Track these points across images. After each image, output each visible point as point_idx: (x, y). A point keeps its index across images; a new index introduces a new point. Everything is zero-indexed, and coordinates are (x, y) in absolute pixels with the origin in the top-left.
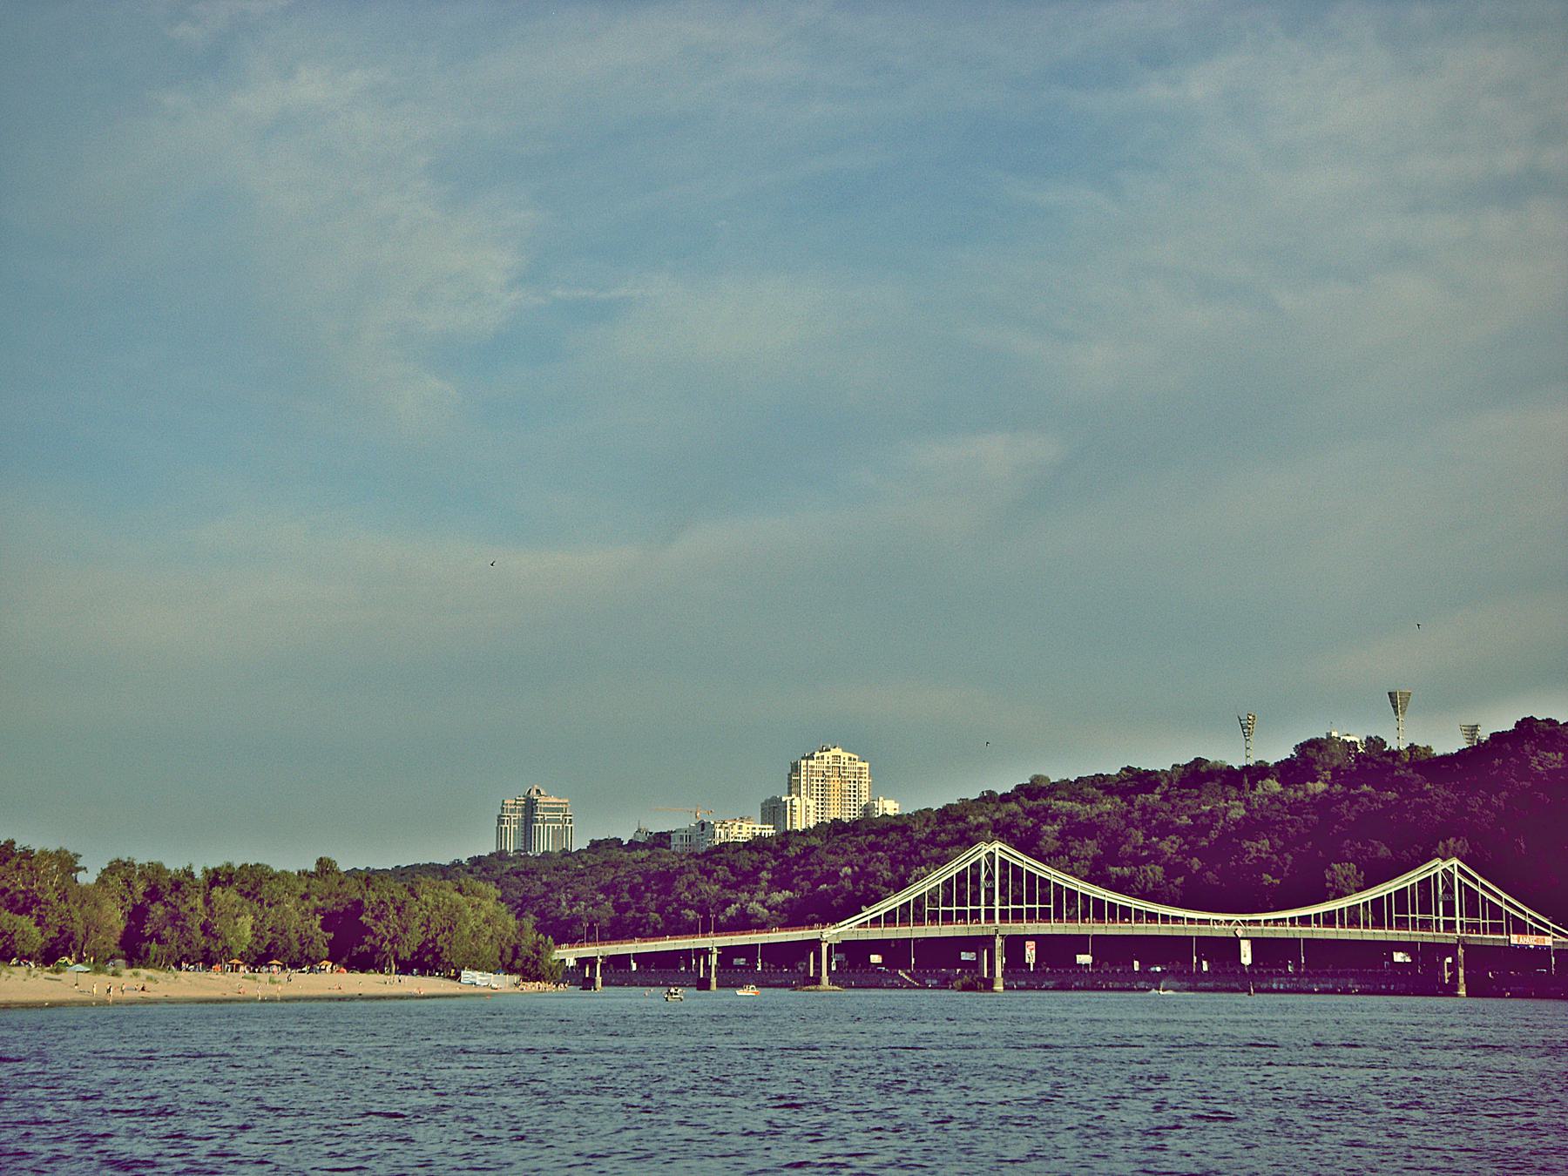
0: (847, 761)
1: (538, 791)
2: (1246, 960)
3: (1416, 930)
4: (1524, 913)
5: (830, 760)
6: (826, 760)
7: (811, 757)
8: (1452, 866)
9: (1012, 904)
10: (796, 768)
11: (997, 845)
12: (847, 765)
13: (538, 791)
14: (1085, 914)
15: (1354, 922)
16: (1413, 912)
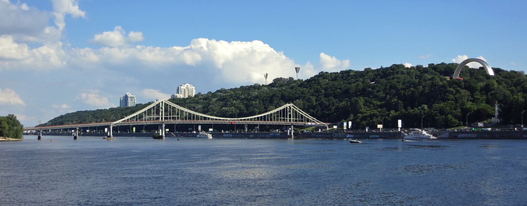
1: (128, 94)
2: (400, 122)
4: (309, 117)
5: (186, 86)
6: (185, 86)
7: (182, 86)
8: (291, 105)
9: (169, 116)
13: (128, 94)
14: (194, 119)
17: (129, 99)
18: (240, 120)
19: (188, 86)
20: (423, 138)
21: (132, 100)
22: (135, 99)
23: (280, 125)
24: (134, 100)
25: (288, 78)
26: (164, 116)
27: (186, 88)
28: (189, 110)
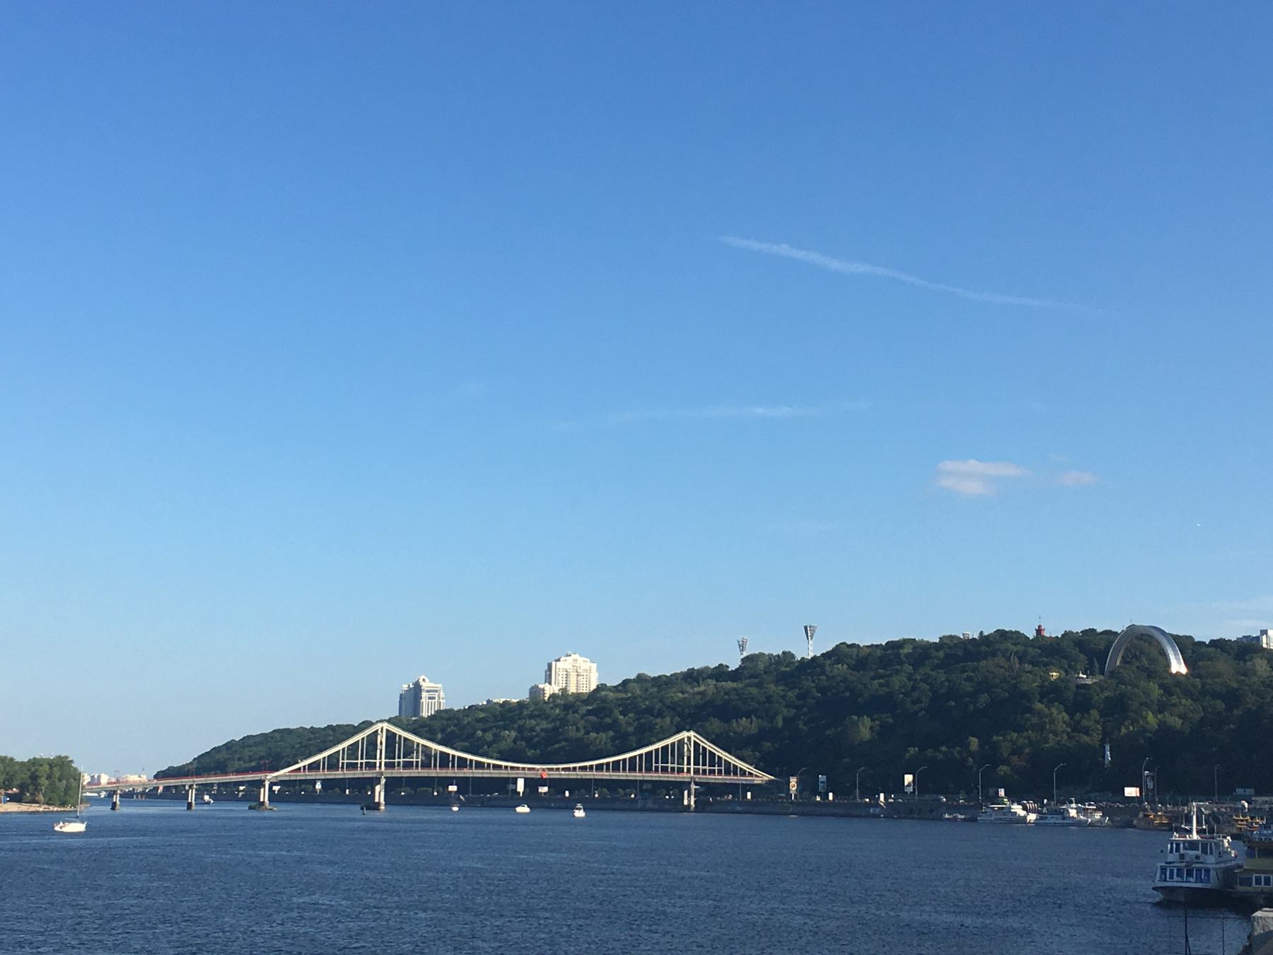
0: (582, 662)
1: (424, 680)
3: (609, 772)
5: (572, 662)
6: (568, 662)
7: (558, 660)
10: (550, 666)
11: (692, 734)
12: (582, 665)
13: (424, 680)
15: (632, 769)
16: (362, 759)
17: (424, 694)
18: (690, 768)
19: (575, 660)
20: (1011, 822)
21: (434, 698)
22: (442, 695)
23: (614, 780)
24: (439, 698)
25: (780, 653)
26: (383, 760)
27: (571, 667)
28: (727, 754)
